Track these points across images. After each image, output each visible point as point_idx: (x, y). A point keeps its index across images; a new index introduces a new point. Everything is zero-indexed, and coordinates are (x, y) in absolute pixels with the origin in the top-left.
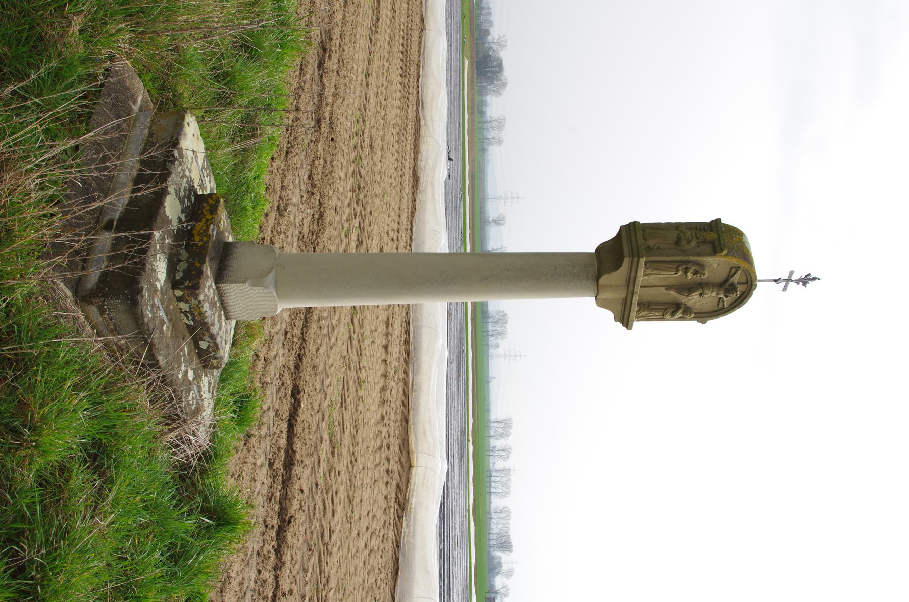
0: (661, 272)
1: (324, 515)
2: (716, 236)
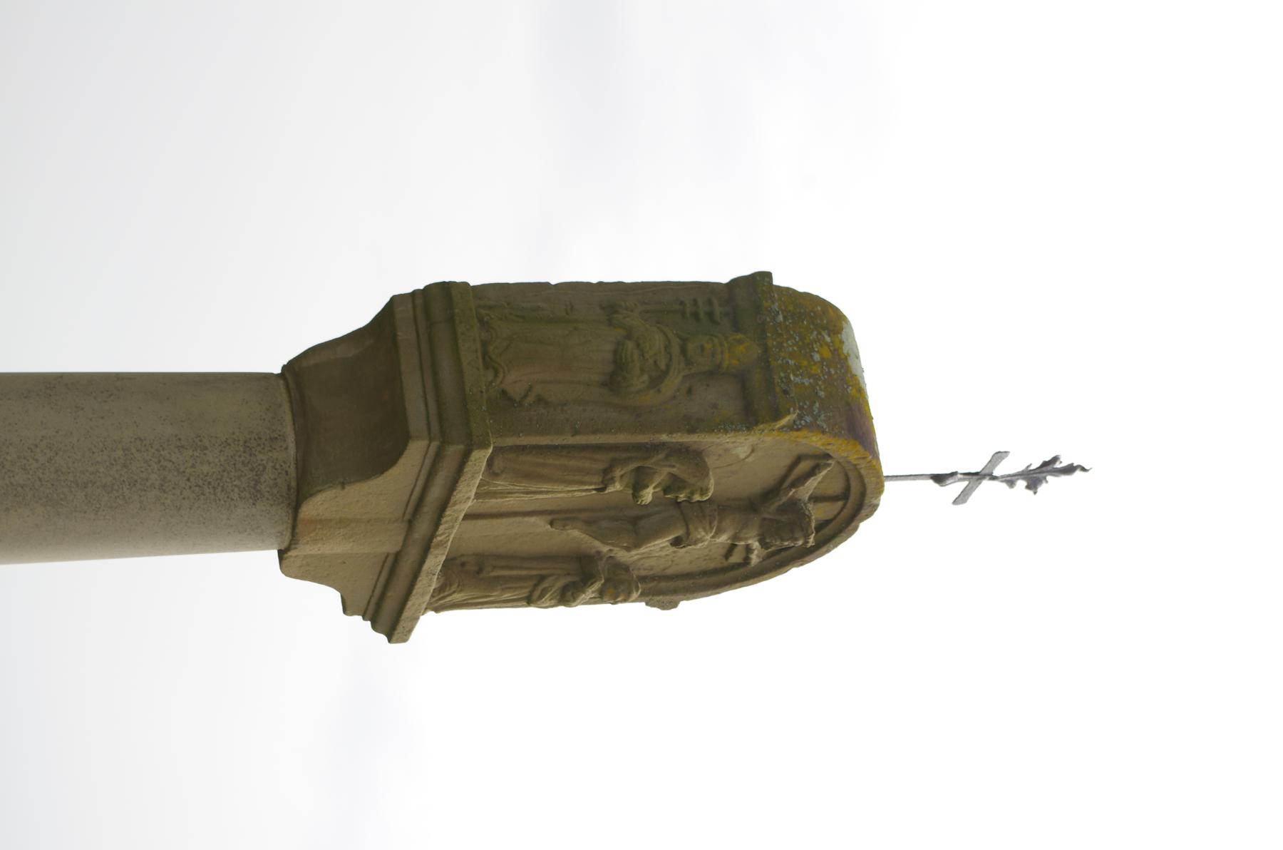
0: (545, 487)
2: (756, 351)
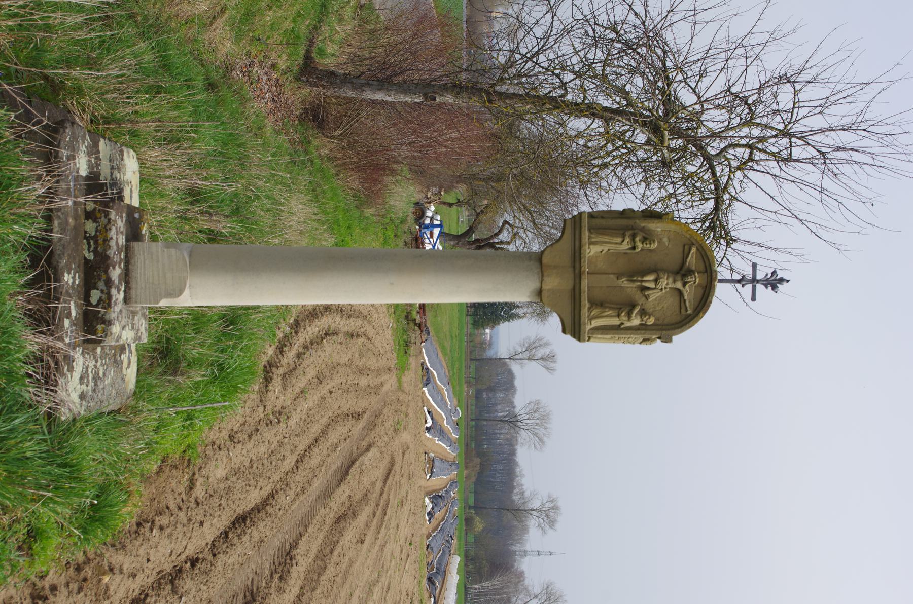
1: (392, 463)
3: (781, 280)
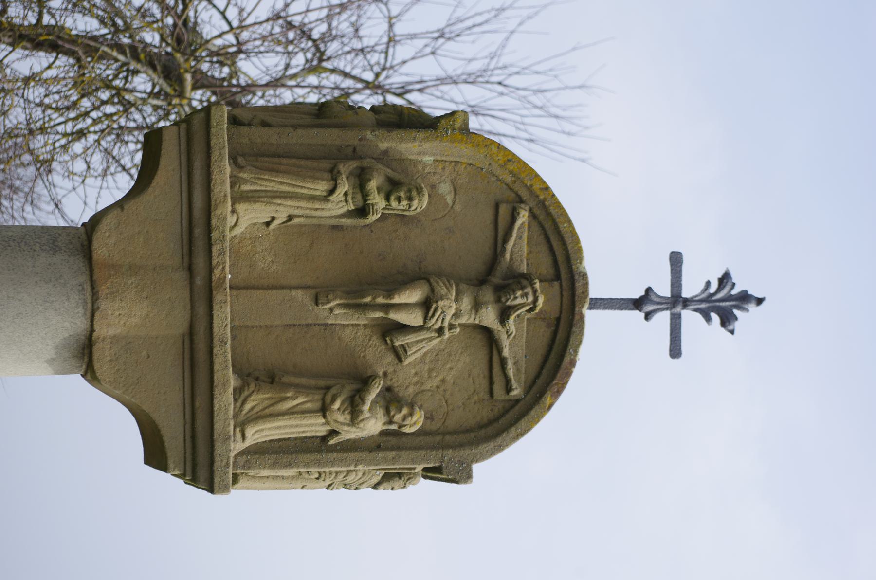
3: (744, 298)
